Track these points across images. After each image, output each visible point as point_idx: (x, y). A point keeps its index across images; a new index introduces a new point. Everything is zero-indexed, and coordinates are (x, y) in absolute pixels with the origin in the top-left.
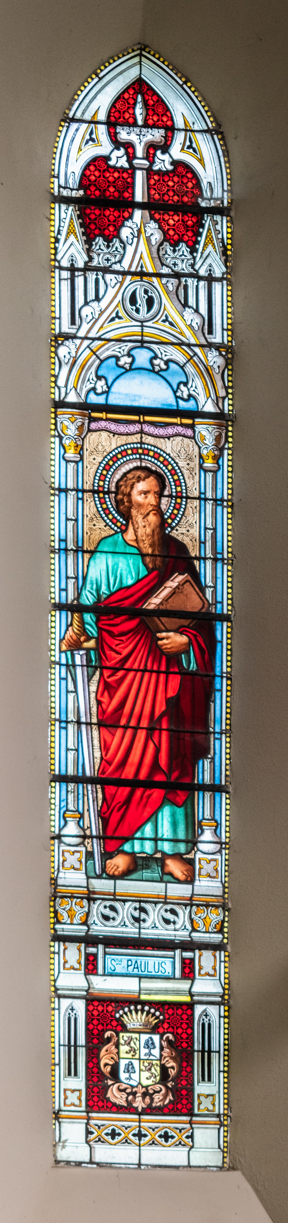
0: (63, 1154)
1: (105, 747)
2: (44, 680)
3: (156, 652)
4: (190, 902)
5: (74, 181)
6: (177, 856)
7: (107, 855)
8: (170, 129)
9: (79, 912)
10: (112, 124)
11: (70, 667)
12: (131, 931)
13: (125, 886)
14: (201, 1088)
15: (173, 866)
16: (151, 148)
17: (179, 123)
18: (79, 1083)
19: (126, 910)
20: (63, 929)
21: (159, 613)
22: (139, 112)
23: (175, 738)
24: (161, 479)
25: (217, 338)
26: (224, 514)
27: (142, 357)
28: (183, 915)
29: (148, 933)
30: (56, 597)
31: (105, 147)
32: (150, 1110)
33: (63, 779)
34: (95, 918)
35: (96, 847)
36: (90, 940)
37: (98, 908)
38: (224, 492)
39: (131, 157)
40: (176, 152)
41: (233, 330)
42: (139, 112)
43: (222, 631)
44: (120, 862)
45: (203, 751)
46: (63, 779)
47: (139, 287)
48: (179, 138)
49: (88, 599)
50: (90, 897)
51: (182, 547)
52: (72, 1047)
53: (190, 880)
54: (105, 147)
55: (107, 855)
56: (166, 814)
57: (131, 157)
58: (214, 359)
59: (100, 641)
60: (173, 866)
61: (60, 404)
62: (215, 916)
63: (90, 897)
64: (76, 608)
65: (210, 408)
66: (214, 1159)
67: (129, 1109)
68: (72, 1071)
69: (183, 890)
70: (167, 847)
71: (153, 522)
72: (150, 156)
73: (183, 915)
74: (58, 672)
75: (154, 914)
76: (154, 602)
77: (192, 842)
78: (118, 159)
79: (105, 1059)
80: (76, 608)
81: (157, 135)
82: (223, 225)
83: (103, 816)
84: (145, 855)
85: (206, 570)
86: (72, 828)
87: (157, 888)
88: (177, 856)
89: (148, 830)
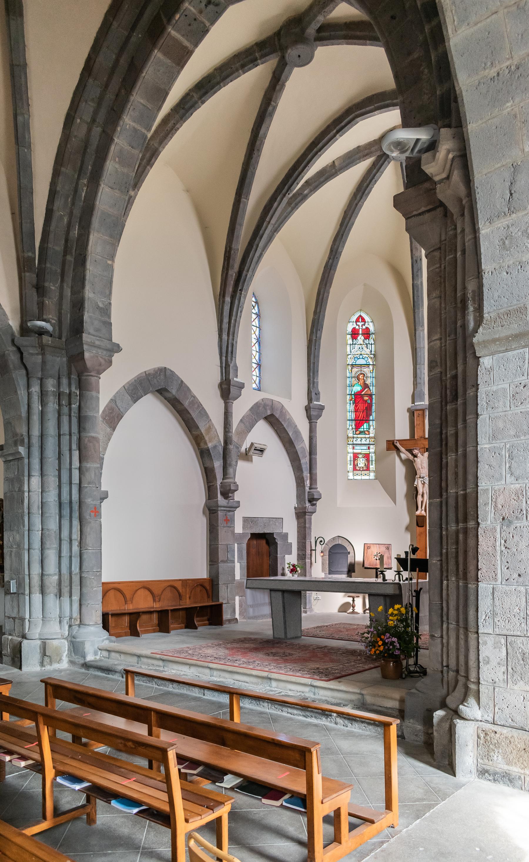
0: (349, 478)
1: (356, 415)
2: (346, 405)
3: (364, 400)
4: (369, 438)
5: (350, 331)
6: (367, 431)
7: (356, 431)
8: (365, 322)
9: (352, 440)
10: (356, 322)
11: (350, 403)
12: (360, 443)
13: (359, 436)
14: (371, 467)
15: (366, 432)
16: (362, 325)
17: (366, 321)
18: (352, 466)
19: (359, 439)
20: (461, 301)
21: (364, 394)
22: (360, 320)
23: (367, 413)
24: (364, 374)
25: (373, 353)
26: (374, 379)
27: (361, 357)
28: (368, 439)
29: (363, 443)
30: (348, 393)
31: (355, 326)
32: (363, 470)
33: (349, 420)
34: (354, 441)
35: (354, 430)
36: (353, 444)
37: (355, 439)
38: (374, 376)
39: (359, 327)
40: (366, 325)
41: (375, 351)
42: (360, 320)
43: (374, 397)
44: (358, 432)
45: (371, 415)
46: (349, 420)
47: (360, 346)
48: (367, 323)
49: (353, 393)
50: (353, 438)
51: (367, 384)
52: (351, 461)
53: (369, 434)
54: (355, 326)
55: (356, 431)
56: (365, 425)
57: (359, 327)
58: (372, 356)
59: (355, 399)
60: (366, 432)
61: (348, 365)
62: (373, 440)
63: (353, 438)
64: (351, 395)
65: (372, 363)
66: (374, 478)
67: (360, 470)
68: (351, 465)
69: (368, 436)
70: (365, 430)
71: (313, 613)
72: (362, 326)
73: (368, 439)
74: (348, 404)
75: (364, 440)
76: (363, 393)
77: (369, 429)
78: (357, 327)
79: (356, 463)
80: (351, 395)
81: (363, 323)
82: (374, 336)
83: (356, 425)
84: (471, 325)
85: (371, 388)
86: (351, 427)
87: (364, 436)
88: (367, 431)
89: (362, 427)
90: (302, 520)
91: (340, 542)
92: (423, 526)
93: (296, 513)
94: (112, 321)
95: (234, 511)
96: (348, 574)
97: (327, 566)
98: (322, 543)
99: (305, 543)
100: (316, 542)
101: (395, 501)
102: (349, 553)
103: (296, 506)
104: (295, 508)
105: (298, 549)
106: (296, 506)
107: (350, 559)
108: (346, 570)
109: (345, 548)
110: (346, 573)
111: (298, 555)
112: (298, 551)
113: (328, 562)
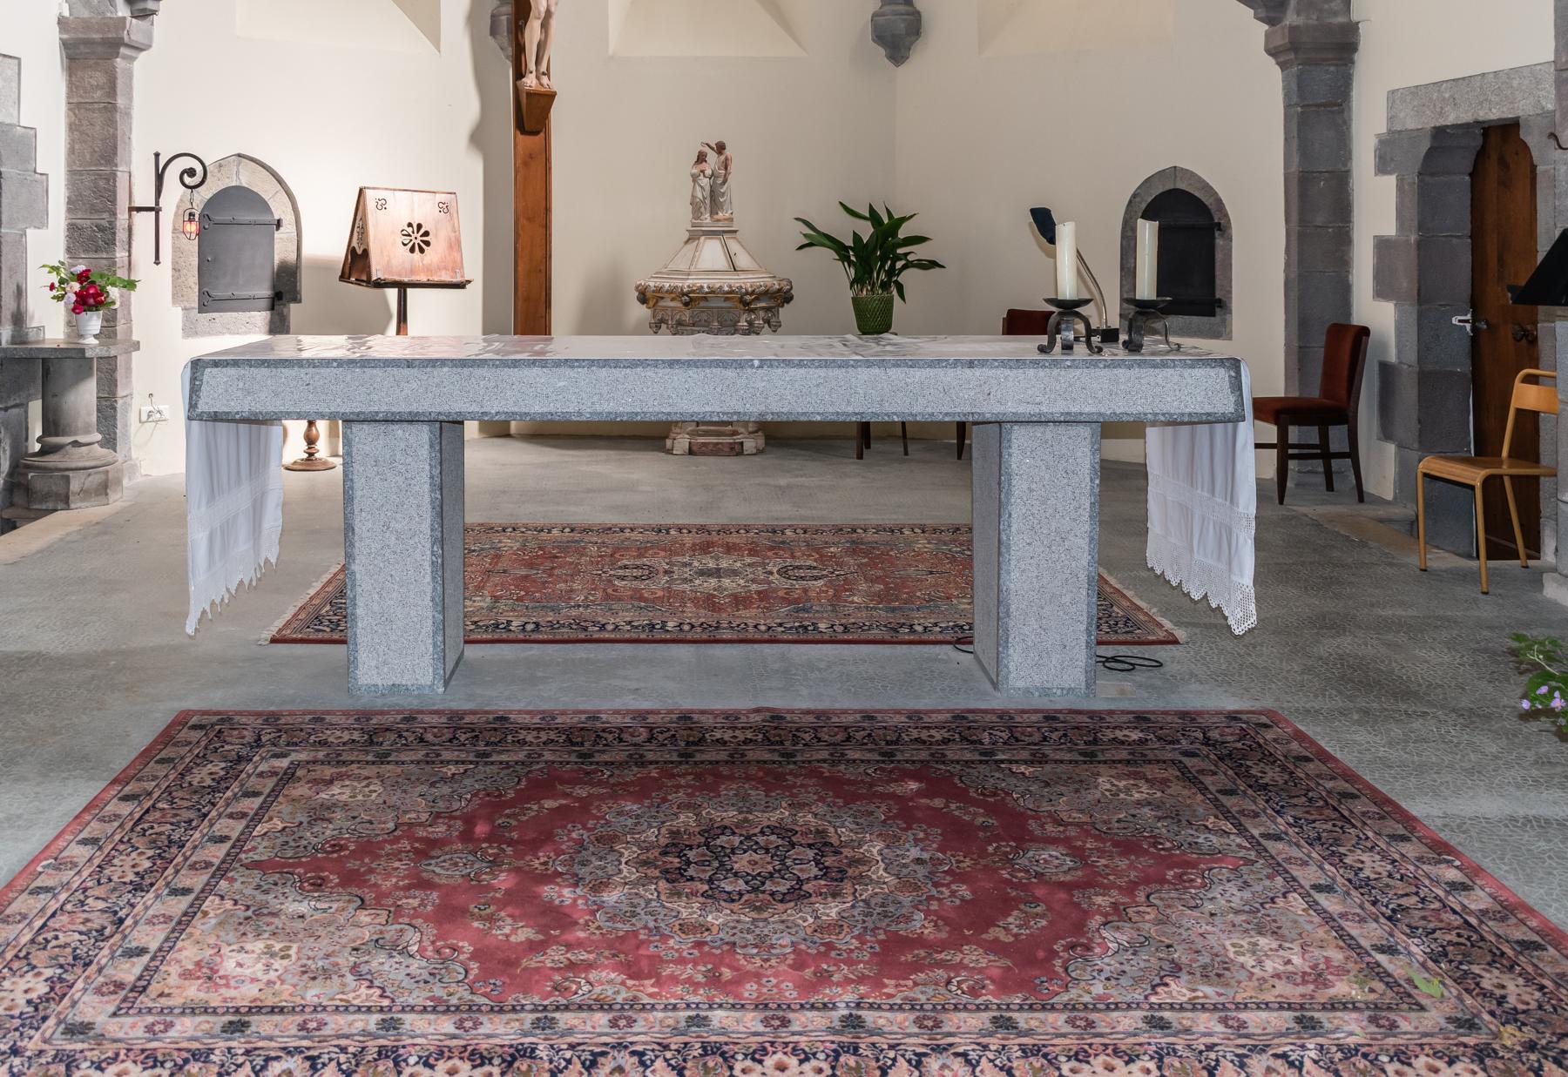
90: (98, 78)
91: (247, 178)
92: (536, 133)
93: (65, 44)
94: (1272, 61)
95: (133, 59)
96: (272, 308)
97: (192, 279)
98: (187, 180)
99: (113, 176)
100: (159, 178)
101: (436, 40)
102: (279, 224)
103: (66, 13)
104: (62, 22)
105: (70, 202)
106: (66, 13)
107: (283, 250)
108: (265, 291)
109: (262, 205)
110: (265, 303)
111: (73, 230)
112: (69, 210)
113: (195, 261)
